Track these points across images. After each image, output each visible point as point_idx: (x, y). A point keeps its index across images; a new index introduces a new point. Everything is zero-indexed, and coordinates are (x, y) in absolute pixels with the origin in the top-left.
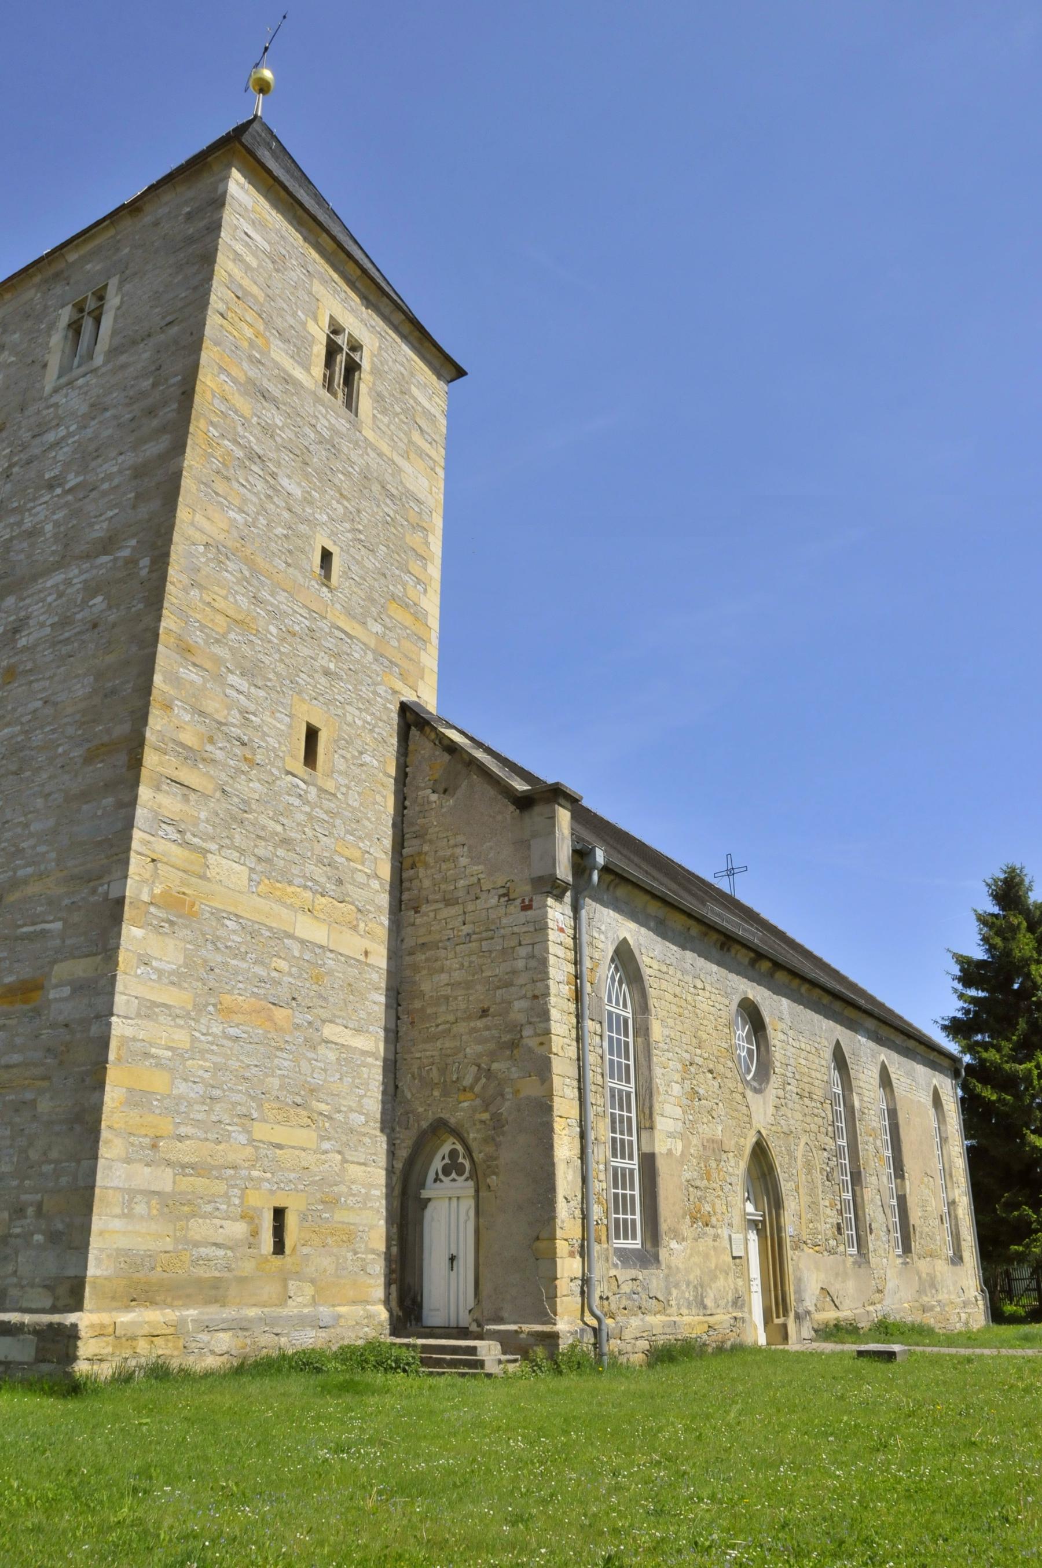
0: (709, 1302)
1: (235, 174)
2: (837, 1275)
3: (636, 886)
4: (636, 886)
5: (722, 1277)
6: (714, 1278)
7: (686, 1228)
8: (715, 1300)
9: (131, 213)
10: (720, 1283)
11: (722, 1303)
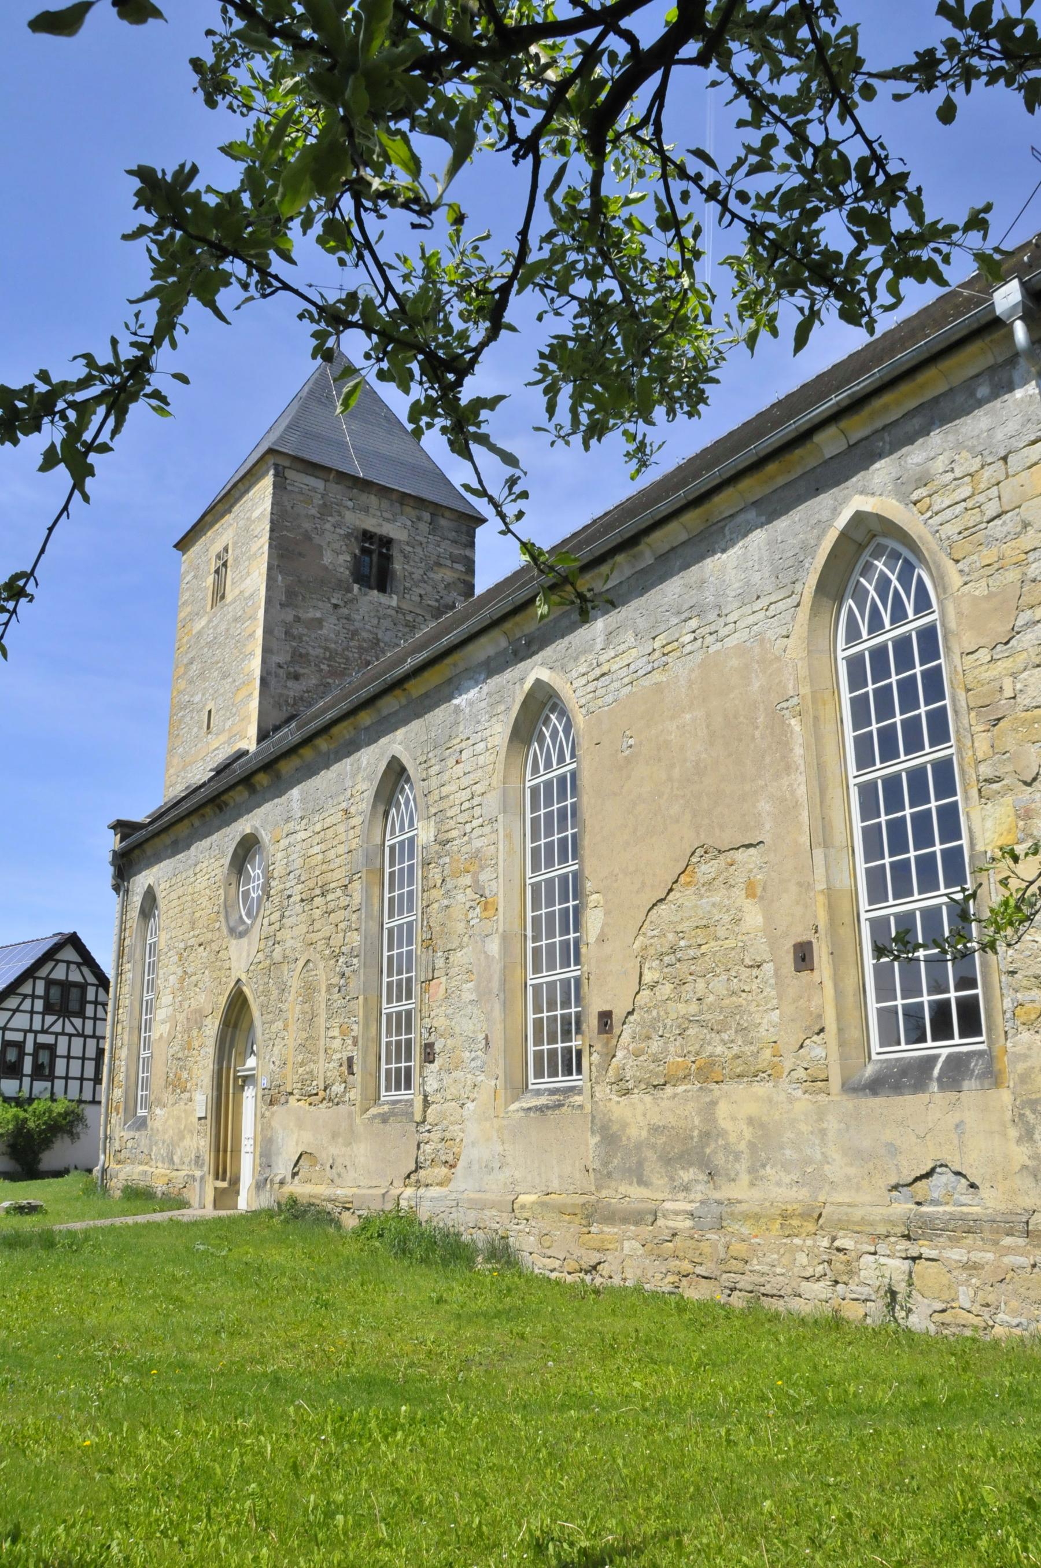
0: (176, 1159)
1: (700, 45)
2: (335, 1135)
3: (147, 840)
4: (147, 840)
5: (188, 1137)
6: (182, 1138)
7: (167, 1097)
8: (181, 1158)
9: (350, 484)
10: (187, 1142)
11: (187, 1160)
